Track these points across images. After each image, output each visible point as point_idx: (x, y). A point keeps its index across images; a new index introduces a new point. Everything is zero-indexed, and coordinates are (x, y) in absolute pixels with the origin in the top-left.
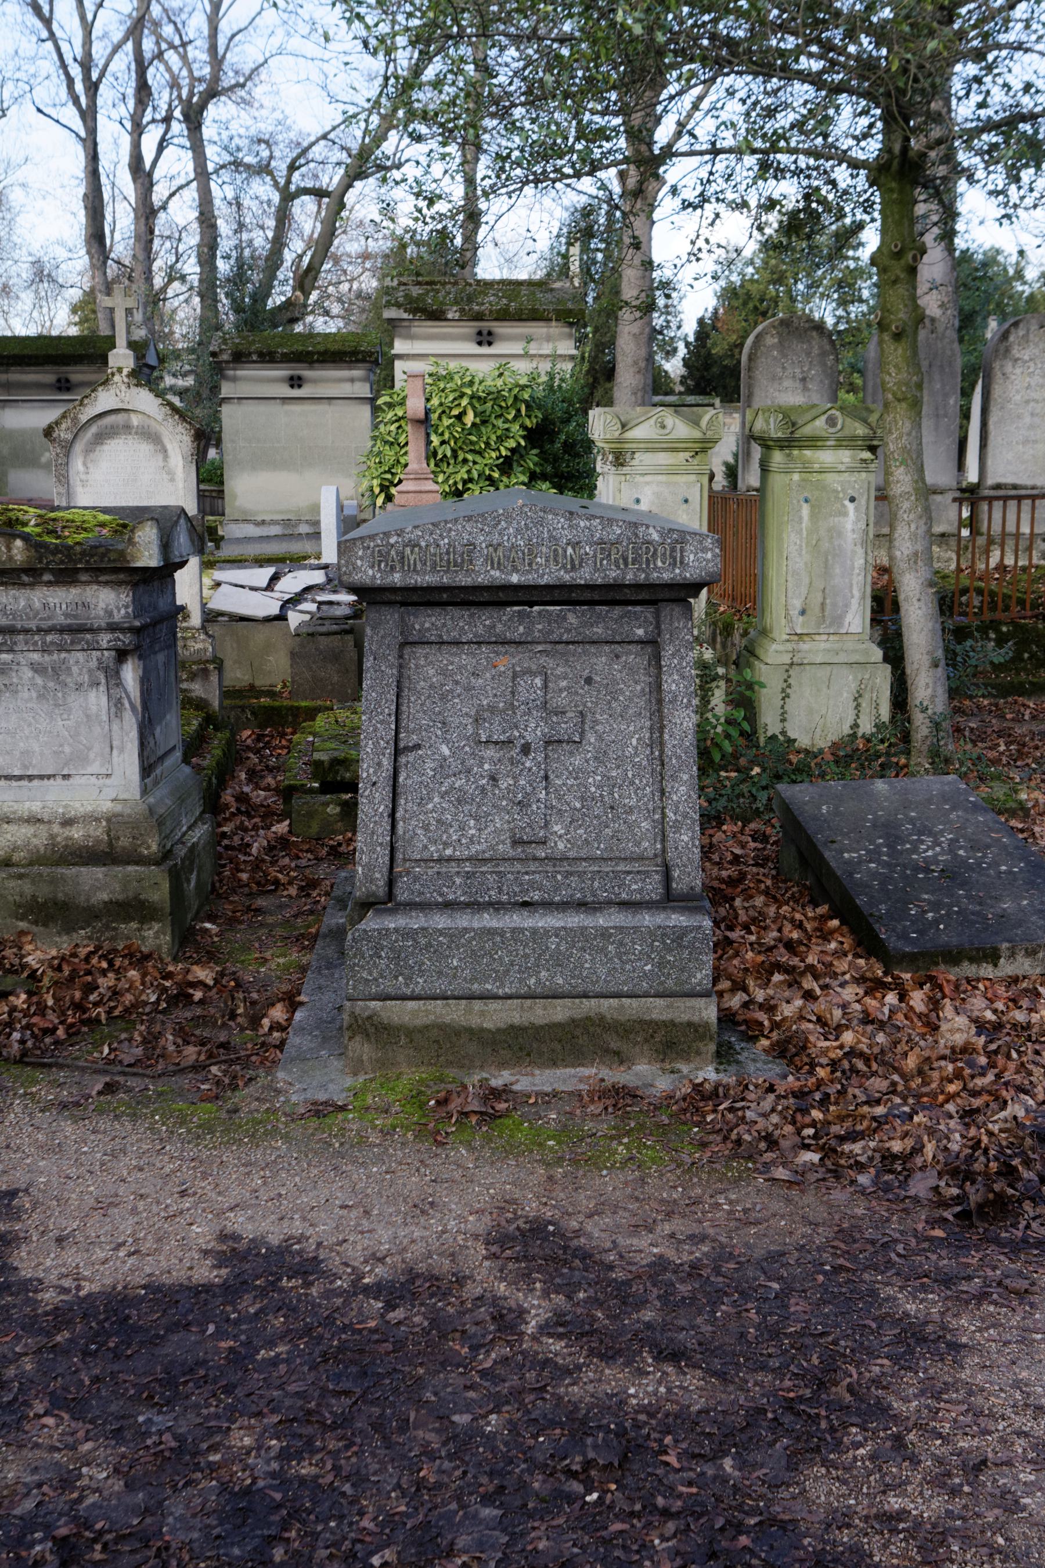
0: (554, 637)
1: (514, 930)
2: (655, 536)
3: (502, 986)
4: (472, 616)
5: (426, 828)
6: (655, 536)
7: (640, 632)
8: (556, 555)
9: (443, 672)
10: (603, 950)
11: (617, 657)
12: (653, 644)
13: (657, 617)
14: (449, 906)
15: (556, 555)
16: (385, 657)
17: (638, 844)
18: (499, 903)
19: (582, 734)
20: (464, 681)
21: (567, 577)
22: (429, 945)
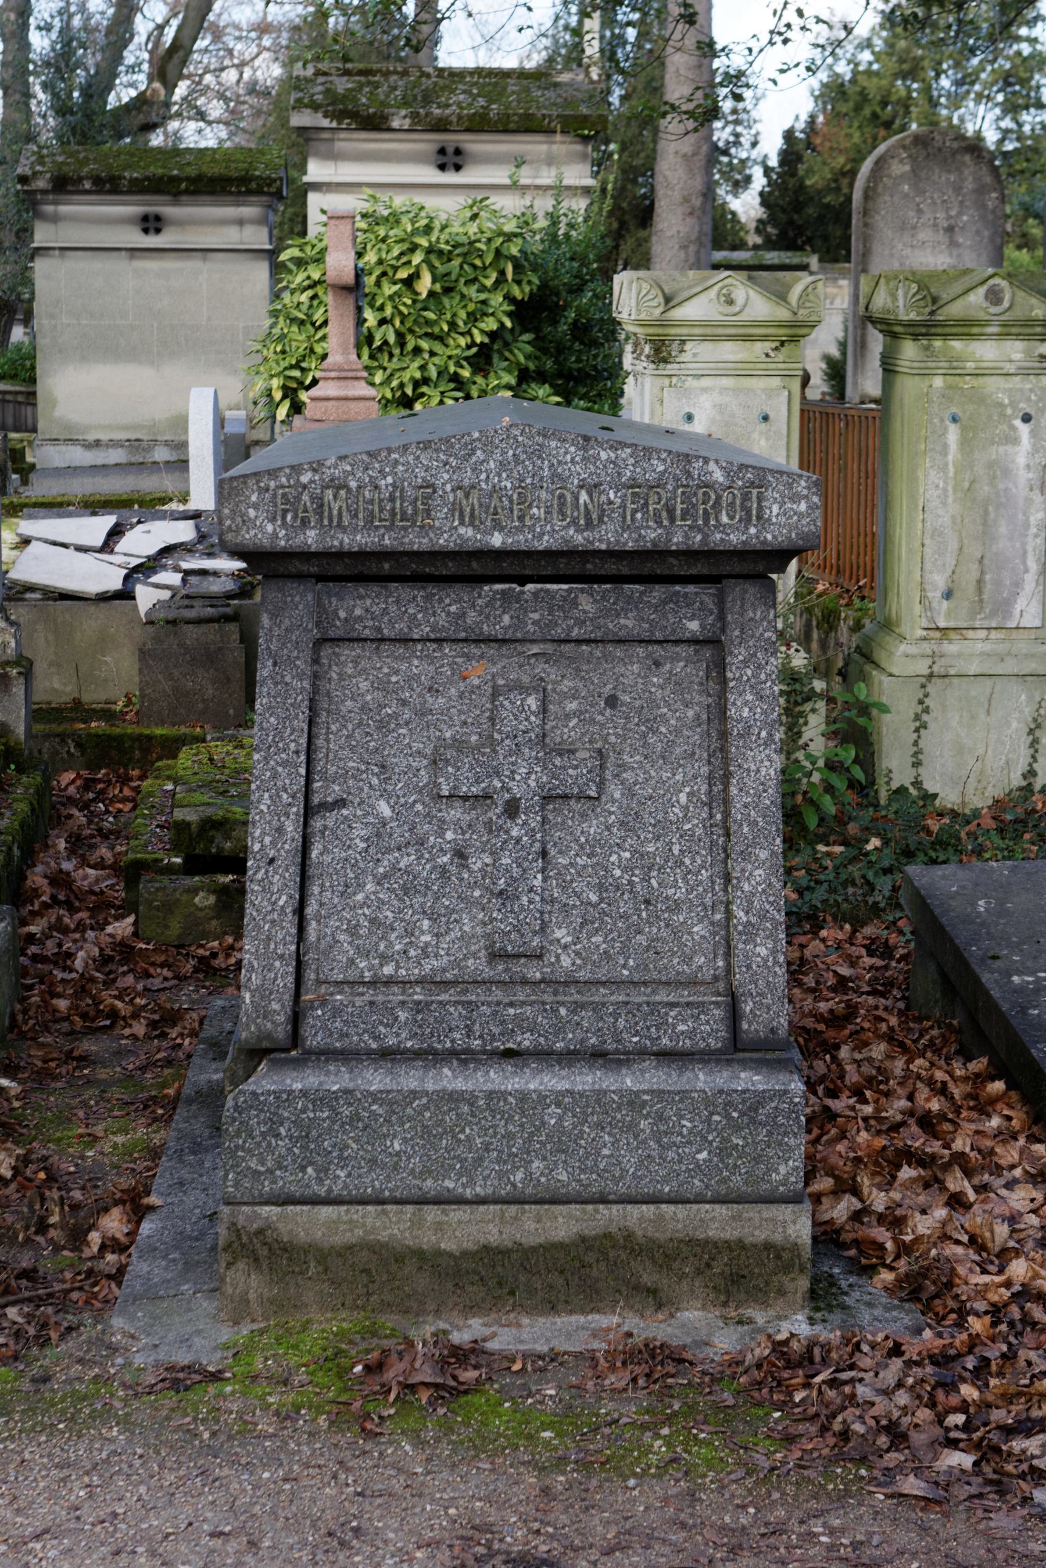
0: (559, 632)
1: (490, 1095)
2: (718, 476)
3: (471, 1182)
4: (428, 598)
5: (353, 931)
6: (718, 476)
7: (694, 626)
8: (562, 504)
9: (382, 686)
10: (632, 1127)
11: (657, 664)
12: (713, 646)
14: (388, 1055)
16: (291, 661)
17: (688, 960)
19: (601, 785)
21: (579, 539)
22: (355, 1117)
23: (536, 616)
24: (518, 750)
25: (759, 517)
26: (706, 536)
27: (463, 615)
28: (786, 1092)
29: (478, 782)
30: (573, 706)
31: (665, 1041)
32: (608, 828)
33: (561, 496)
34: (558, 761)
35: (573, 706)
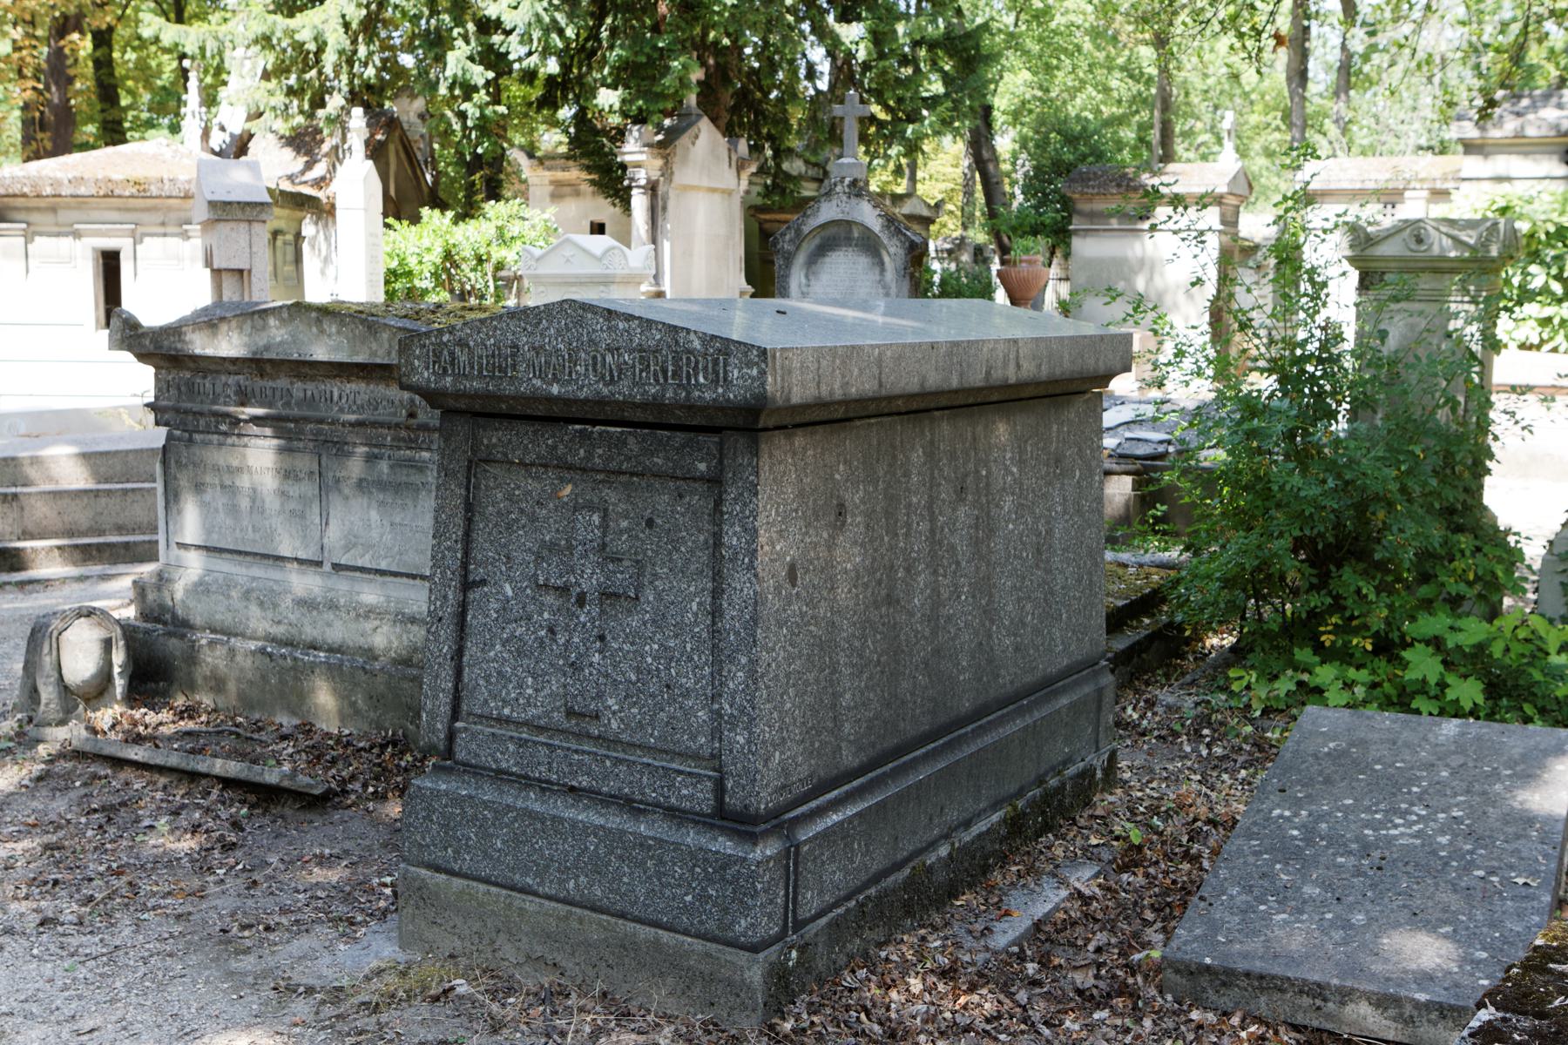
0: (613, 465)
1: (554, 818)
2: (697, 344)
3: (541, 883)
4: (535, 432)
5: (487, 678)
6: (697, 344)
7: (702, 467)
8: (595, 364)
9: (509, 497)
10: (643, 863)
11: (681, 496)
12: (715, 482)
13: (721, 444)
14: (500, 776)
15: (595, 364)
16: (455, 474)
17: (693, 738)
18: (548, 782)
19: (639, 588)
20: (529, 510)
21: (605, 391)
22: (475, 818)
23: (600, 451)
24: (585, 556)
25: (725, 379)
26: (688, 393)
27: (555, 447)
28: (745, 859)
29: (561, 576)
30: (624, 524)
31: (673, 800)
32: (645, 624)
33: (595, 358)
34: (611, 566)
35: (624, 524)
